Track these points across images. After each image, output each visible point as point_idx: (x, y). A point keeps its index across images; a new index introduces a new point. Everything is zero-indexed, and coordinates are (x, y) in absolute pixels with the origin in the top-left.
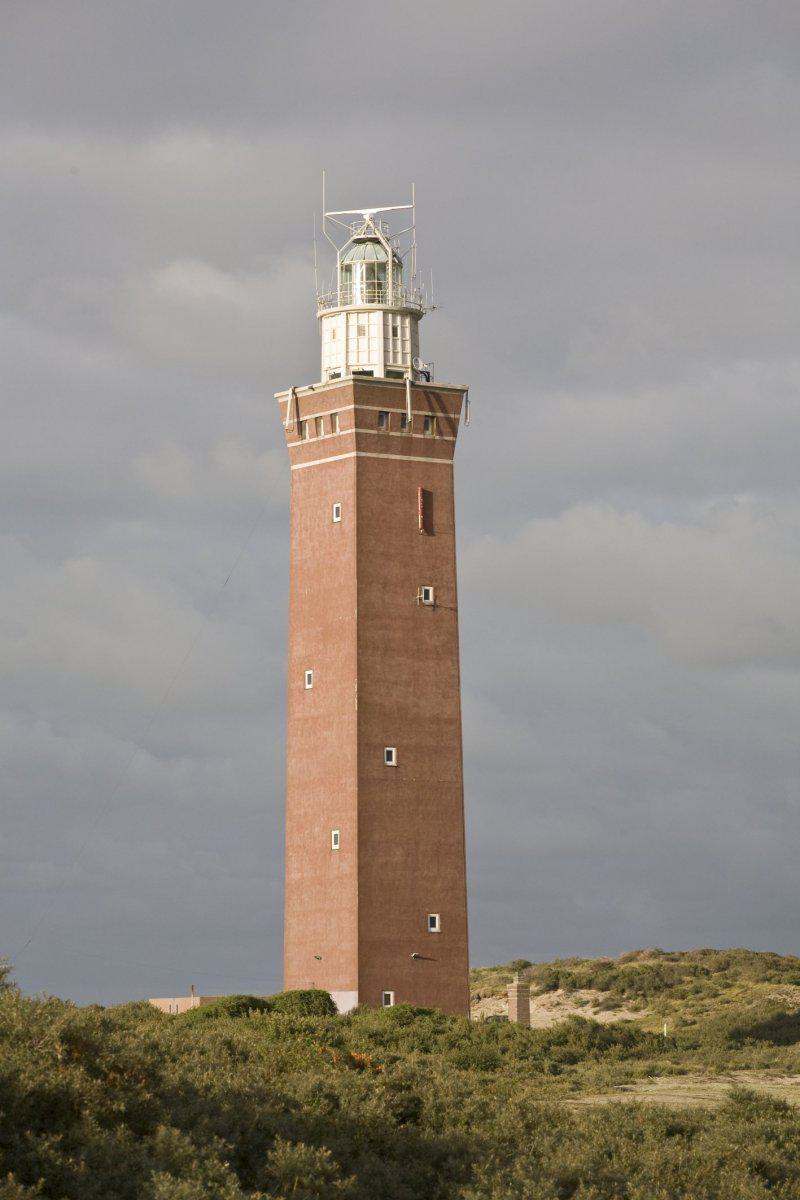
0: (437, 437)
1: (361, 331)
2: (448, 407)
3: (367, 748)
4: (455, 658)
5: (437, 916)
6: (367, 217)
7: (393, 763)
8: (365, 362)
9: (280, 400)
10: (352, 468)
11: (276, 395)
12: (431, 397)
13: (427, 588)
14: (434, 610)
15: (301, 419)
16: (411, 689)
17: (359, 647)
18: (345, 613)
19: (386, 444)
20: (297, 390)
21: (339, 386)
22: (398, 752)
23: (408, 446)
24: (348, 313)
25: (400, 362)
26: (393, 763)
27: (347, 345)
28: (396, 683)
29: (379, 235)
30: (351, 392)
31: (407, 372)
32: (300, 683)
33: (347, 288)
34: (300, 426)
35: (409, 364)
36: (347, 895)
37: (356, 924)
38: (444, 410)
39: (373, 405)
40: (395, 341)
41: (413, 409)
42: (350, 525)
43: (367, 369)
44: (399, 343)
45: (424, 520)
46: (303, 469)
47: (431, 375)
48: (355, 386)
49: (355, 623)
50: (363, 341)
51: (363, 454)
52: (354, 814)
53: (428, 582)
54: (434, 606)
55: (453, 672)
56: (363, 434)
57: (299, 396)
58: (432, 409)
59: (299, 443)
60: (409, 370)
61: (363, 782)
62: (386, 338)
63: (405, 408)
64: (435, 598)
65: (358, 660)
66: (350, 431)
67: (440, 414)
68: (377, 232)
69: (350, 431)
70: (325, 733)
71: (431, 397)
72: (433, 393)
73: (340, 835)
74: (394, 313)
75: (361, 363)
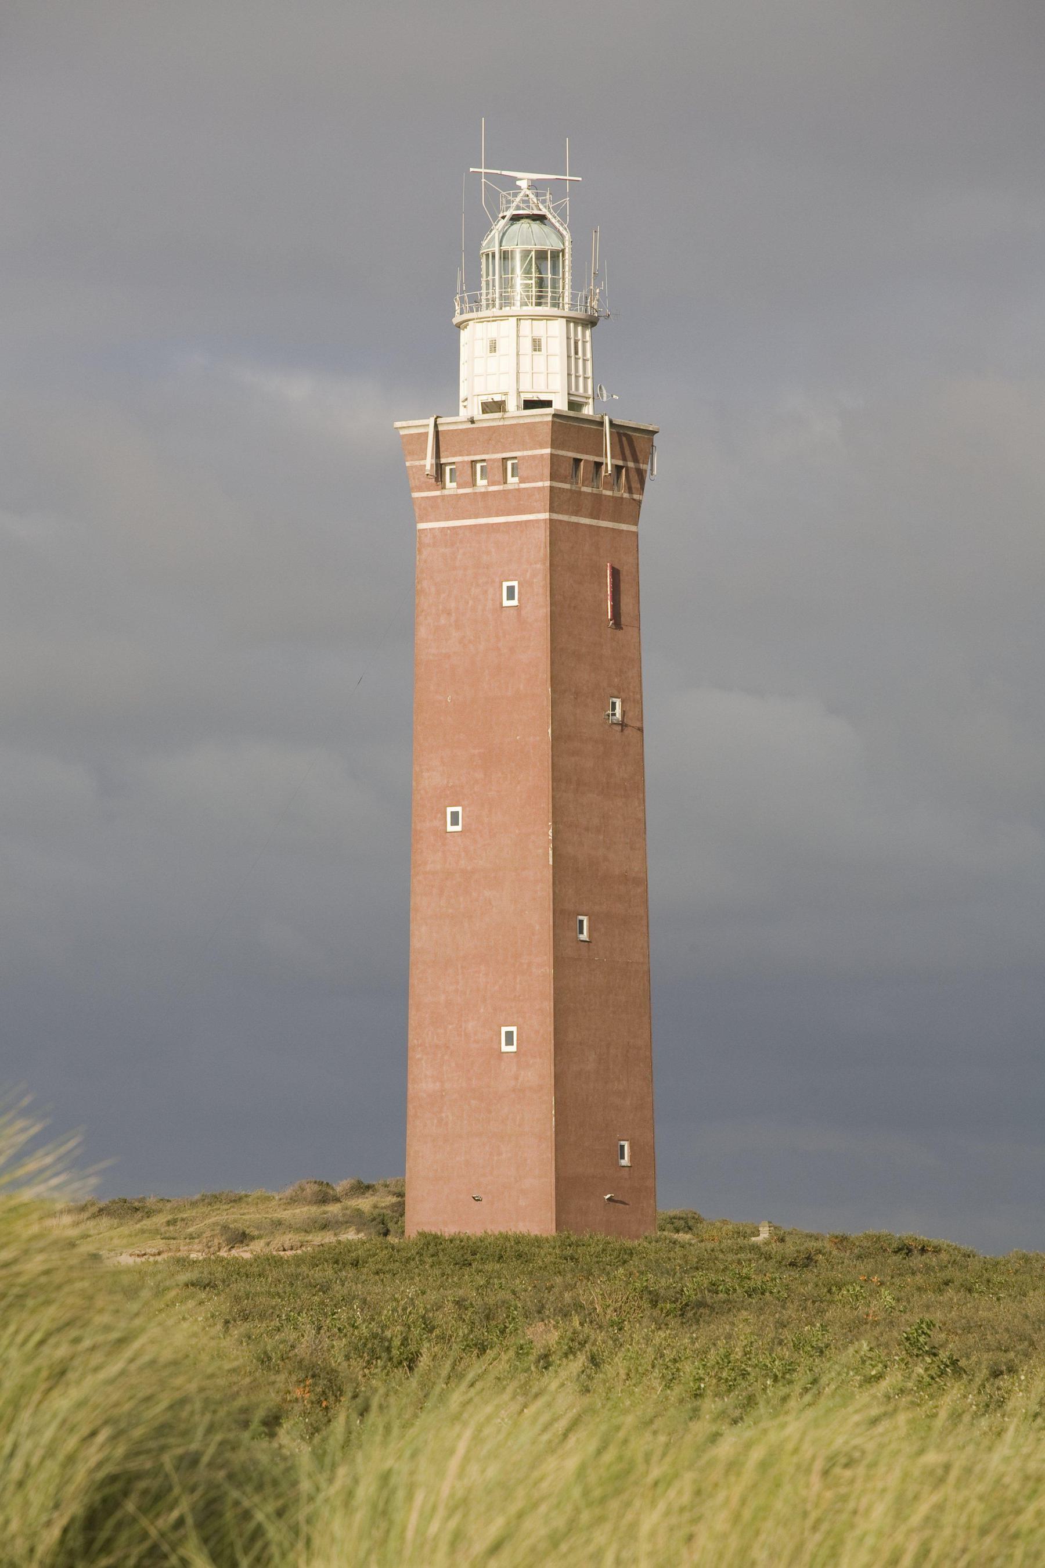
0: (626, 495)
1: (537, 345)
2: (640, 457)
3: (563, 918)
4: (641, 796)
5: (626, 1144)
6: (523, 184)
7: (584, 936)
8: (543, 388)
9: (402, 432)
10: (542, 536)
11: (398, 424)
12: (624, 439)
13: (614, 700)
14: (622, 731)
15: (443, 461)
16: (601, 837)
17: (554, 779)
18: (532, 732)
20: (439, 421)
21: (522, 421)
22: (590, 920)
24: (519, 319)
25: (581, 390)
26: (584, 936)
27: (518, 364)
28: (587, 829)
29: (544, 211)
30: (548, 429)
31: (587, 403)
32: (437, 823)
33: (507, 283)
34: (440, 468)
35: (590, 392)
36: (538, 1116)
37: (550, 1155)
38: (636, 460)
40: (577, 359)
41: (612, 457)
42: (539, 611)
43: (544, 397)
44: (580, 362)
45: (613, 607)
46: (442, 530)
47: (488, 399)
48: (553, 422)
49: (547, 748)
50: (540, 358)
51: (555, 516)
52: (549, 1006)
53: (616, 693)
54: (623, 725)
55: (640, 815)
57: (440, 428)
58: (624, 459)
59: (437, 493)
60: (591, 401)
61: (559, 962)
62: (569, 357)
63: (599, 451)
64: (624, 713)
65: (553, 797)
66: (540, 484)
67: (631, 464)
68: (541, 207)
69: (540, 484)
70: (487, 893)
71: (624, 439)
72: (625, 435)
73: (518, 1039)
74: (576, 321)
75: (551, 388)
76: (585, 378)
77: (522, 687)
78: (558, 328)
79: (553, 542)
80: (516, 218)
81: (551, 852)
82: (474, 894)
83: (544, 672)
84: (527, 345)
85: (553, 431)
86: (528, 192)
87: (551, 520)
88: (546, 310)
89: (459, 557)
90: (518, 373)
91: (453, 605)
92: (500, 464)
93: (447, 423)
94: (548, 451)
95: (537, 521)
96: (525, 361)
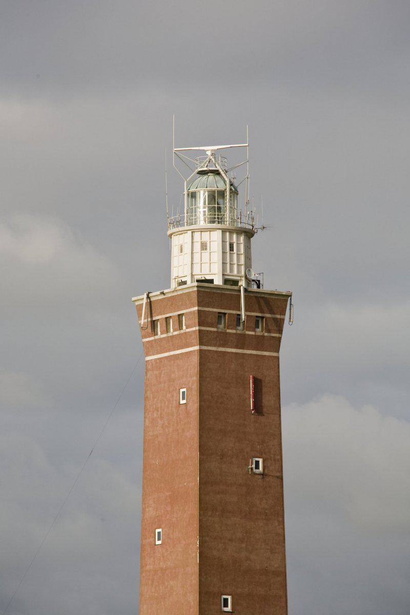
1: (204, 246)
6: (209, 153)
10: (195, 359)
13: (257, 459)
14: (263, 478)
16: (244, 545)
17: (201, 509)
19: (223, 339)
20: (151, 295)
22: (233, 599)
23: (242, 342)
25: (235, 272)
28: (231, 540)
29: (218, 168)
33: (192, 211)
39: (213, 307)
41: (246, 310)
42: (194, 407)
43: (208, 277)
45: (254, 403)
46: (156, 360)
48: (198, 291)
49: (197, 489)
50: (206, 255)
54: (263, 475)
56: (205, 331)
60: (243, 279)
62: (224, 253)
64: (264, 469)
66: (194, 329)
68: (217, 165)
69: (194, 329)
70: (172, 583)
75: (213, 272)
76: (239, 265)
77: (187, 452)
78: (217, 236)
79: (202, 364)
80: (202, 173)
81: (198, 555)
82: (166, 584)
83: (196, 445)
84: (197, 246)
85: (199, 296)
86: (211, 157)
87: (200, 350)
88: (215, 225)
89: (162, 375)
90: (192, 264)
91: (159, 406)
92: (177, 318)
93: (156, 295)
94: (196, 308)
95: (194, 351)
96: (197, 257)
